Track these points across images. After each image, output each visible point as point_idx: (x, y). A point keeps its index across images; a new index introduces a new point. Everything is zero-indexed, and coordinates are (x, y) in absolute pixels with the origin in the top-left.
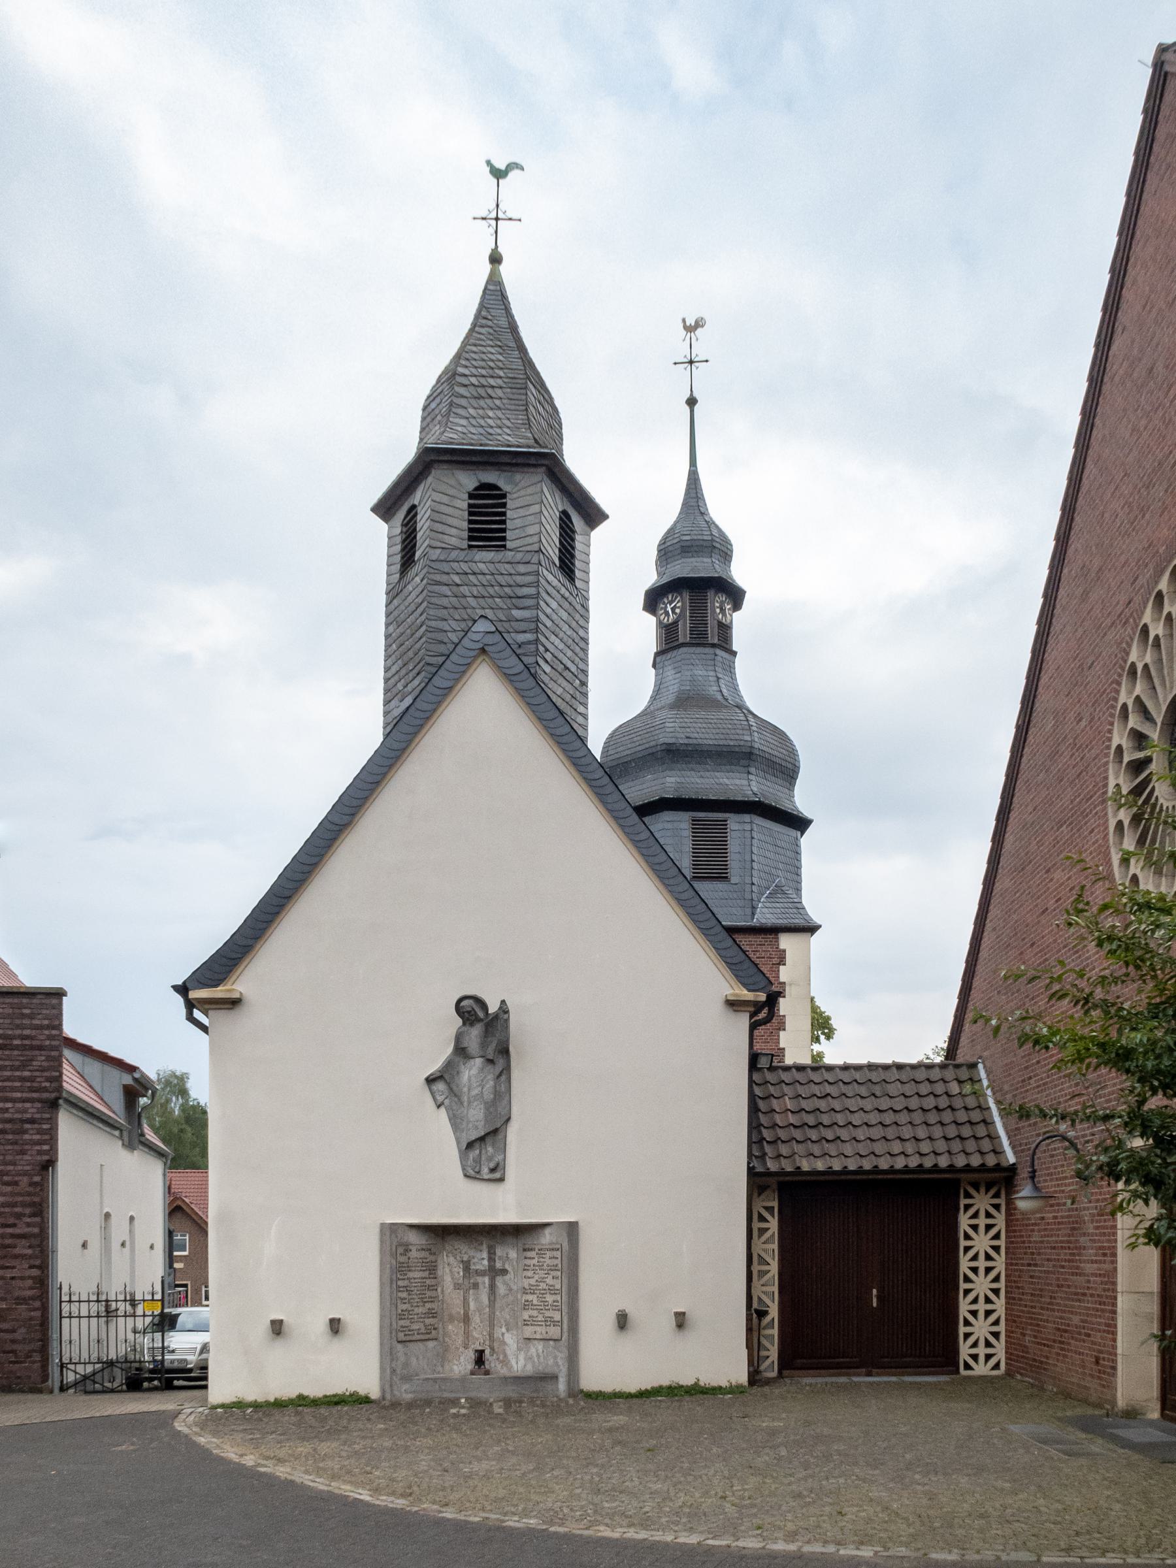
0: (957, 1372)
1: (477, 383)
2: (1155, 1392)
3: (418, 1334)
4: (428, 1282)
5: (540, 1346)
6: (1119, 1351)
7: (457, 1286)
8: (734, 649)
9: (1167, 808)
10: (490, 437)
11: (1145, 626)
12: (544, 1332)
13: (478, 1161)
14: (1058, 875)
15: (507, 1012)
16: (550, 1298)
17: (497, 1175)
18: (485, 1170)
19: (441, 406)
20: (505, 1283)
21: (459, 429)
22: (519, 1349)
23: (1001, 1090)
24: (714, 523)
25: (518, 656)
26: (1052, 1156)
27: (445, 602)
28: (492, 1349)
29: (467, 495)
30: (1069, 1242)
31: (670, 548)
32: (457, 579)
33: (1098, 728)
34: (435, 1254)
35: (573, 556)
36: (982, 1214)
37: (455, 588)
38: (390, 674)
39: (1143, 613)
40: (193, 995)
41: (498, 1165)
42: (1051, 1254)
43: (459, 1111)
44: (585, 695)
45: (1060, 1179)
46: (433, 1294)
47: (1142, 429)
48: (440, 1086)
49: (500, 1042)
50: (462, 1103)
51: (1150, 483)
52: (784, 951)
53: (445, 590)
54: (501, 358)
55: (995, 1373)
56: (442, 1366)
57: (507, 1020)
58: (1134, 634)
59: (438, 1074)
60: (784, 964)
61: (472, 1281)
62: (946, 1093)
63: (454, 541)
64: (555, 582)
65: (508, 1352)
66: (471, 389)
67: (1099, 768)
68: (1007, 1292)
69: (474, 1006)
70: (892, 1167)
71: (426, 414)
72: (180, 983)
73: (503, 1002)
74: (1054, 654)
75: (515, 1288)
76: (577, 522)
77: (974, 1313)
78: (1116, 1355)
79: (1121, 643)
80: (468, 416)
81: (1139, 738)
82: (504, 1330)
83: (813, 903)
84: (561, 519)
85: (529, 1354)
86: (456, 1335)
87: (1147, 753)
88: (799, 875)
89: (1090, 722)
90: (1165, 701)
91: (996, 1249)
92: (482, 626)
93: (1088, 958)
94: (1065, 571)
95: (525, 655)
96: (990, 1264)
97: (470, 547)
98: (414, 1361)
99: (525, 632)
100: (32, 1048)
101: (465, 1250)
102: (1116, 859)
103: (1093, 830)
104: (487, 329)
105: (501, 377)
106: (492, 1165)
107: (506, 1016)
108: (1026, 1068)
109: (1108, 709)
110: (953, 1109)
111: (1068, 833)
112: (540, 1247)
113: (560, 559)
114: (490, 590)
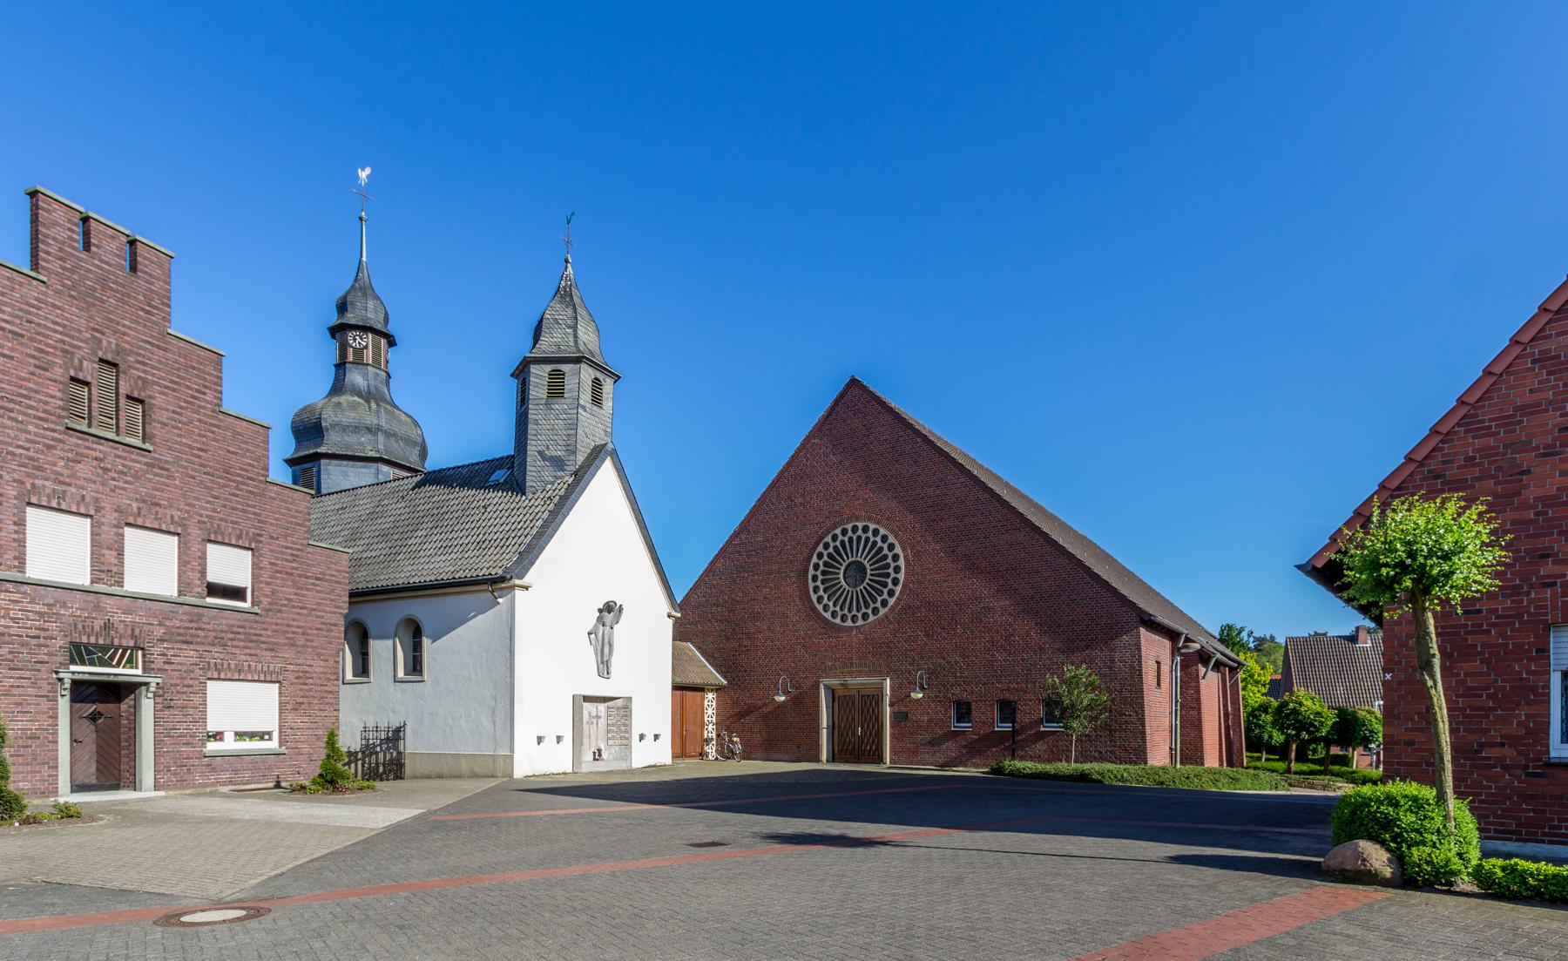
16: (623, 728)
18: (606, 673)
48: (593, 636)
100: (336, 582)
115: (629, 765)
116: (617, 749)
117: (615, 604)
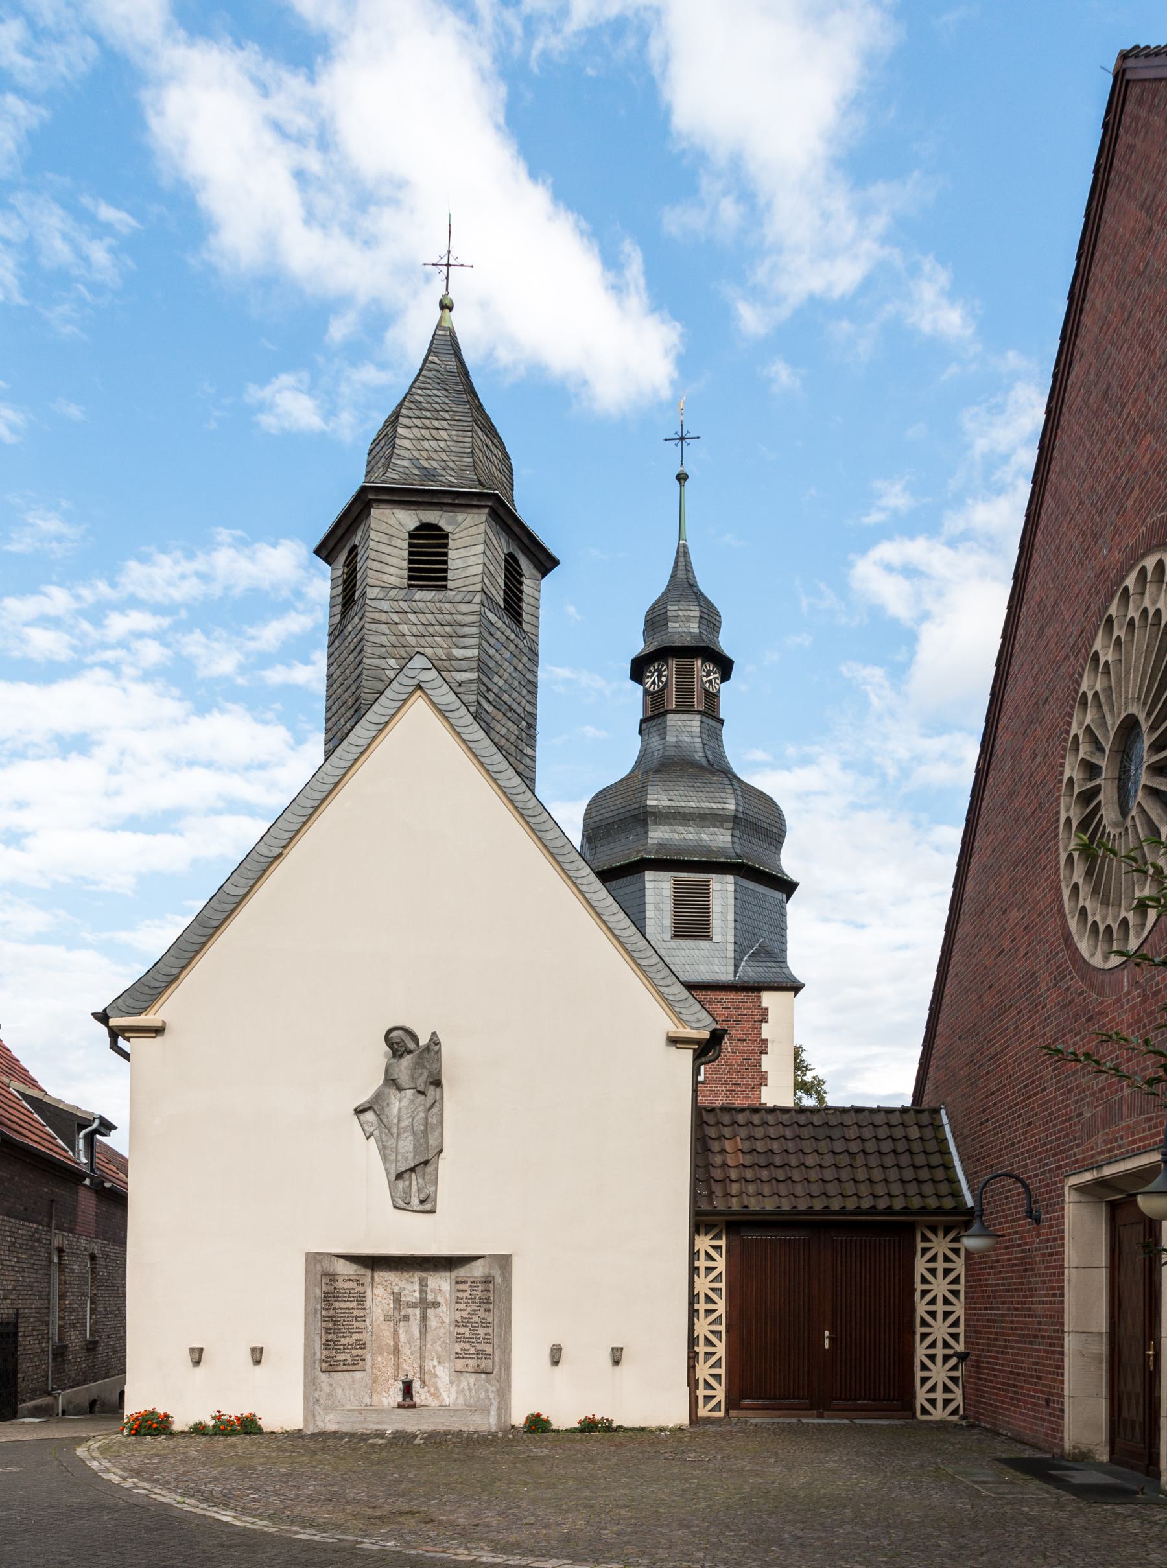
0: (914, 1416)
1: (420, 425)
2: (1103, 1436)
3: (345, 1365)
4: (356, 1313)
5: (471, 1379)
6: (1066, 1393)
7: (387, 1318)
8: (721, 716)
9: (1114, 835)
10: (432, 478)
11: (1096, 653)
12: (475, 1365)
13: (407, 1192)
14: (1014, 914)
15: (437, 1044)
16: (481, 1331)
17: (428, 1207)
18: (415, 1201)
19: (384, 450)
20: (437, 1316)
21: (401, 470)
22: (451, 1383)
23: (962, 1134)
24: (702, 594)
25: (455, 693)
26: (1007, 1198)
27: (383, 640)
28: (423, 1382)
29: (407, 536)
30: (1022, 1284)
31: (658, 619)
32: (396, 618)
33: (1051, 763)
34: (363, 1285)
35: (520, 600)
36: (940, 1258)
37: (393, 627)
38: (330, 714)
39: (1094, 640)
40: (113, 1022)
41: (428, 1196)
42: (1005, 1297)
43: (389, 1143)
44: (534, 737)
45: (1014, 1221)
46: (361, 1325)
47: (1096, 454)
48: (370, 1116)
49: (431, 1074)
50: (392, 1135)
51: (1102, 509)
52: (767, 1009)
53: (384, 628)
54: (447, 401)
55: (955, 1418)
56: (371, 1397)
57: (438, 1052)
58: (1086, 664)
59: (368, 1105)
60: (767, 1022)
61: (402, 1313)
62: (905, 1137)
63: (393, 580)
64: (499, 624)
65: (439, 1385)
66: (415, 430)
67: (1051, 804)
68: (966, 1337)
69: (404, 1038)
70: (844, 1207)
71: (370, 458)
72: (100, 1010)
73: (434, 1034)
74: (1012, 695)
75: (447, 1320)
76: (525, 565)
77: (932, 1358)
78: (1062, 1396)
79: (1073, 675)
80: (411, 457)
81: (1091, 770)
82: (435, 1362)
83: (797, 963)
84: (506, 561)
85: (461, 1387)
86: (386, 1366)
87: (1097, 782)
88: (784, 936)
89: (1044, 758)
90: (1112, 728)
91: (955, 1293)
92: (419, 662)
93: (1041, 995)
94: (1024, 610)
95: (463, 693)
96: (949, 1308)
97: (410, 586)
98: (339, 1392)
99: (465, 671)
101: (409, 1285)
102: (1066, 893)
103: (1045, 867)
104: (434, 373)
105: (446, 420)
106: (422, 1197)
107: (436, 1048)
108: (984, 1111)
109: (1060, 743)
110: (912, 1153)
111: (1023, 872)
112: (472, 1280)
113: (505, 600)
114: (431, 629)
115: (493, 1420)
116: (472, 1381)
117: (414, 1037)
